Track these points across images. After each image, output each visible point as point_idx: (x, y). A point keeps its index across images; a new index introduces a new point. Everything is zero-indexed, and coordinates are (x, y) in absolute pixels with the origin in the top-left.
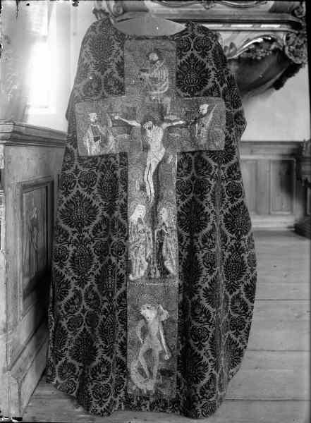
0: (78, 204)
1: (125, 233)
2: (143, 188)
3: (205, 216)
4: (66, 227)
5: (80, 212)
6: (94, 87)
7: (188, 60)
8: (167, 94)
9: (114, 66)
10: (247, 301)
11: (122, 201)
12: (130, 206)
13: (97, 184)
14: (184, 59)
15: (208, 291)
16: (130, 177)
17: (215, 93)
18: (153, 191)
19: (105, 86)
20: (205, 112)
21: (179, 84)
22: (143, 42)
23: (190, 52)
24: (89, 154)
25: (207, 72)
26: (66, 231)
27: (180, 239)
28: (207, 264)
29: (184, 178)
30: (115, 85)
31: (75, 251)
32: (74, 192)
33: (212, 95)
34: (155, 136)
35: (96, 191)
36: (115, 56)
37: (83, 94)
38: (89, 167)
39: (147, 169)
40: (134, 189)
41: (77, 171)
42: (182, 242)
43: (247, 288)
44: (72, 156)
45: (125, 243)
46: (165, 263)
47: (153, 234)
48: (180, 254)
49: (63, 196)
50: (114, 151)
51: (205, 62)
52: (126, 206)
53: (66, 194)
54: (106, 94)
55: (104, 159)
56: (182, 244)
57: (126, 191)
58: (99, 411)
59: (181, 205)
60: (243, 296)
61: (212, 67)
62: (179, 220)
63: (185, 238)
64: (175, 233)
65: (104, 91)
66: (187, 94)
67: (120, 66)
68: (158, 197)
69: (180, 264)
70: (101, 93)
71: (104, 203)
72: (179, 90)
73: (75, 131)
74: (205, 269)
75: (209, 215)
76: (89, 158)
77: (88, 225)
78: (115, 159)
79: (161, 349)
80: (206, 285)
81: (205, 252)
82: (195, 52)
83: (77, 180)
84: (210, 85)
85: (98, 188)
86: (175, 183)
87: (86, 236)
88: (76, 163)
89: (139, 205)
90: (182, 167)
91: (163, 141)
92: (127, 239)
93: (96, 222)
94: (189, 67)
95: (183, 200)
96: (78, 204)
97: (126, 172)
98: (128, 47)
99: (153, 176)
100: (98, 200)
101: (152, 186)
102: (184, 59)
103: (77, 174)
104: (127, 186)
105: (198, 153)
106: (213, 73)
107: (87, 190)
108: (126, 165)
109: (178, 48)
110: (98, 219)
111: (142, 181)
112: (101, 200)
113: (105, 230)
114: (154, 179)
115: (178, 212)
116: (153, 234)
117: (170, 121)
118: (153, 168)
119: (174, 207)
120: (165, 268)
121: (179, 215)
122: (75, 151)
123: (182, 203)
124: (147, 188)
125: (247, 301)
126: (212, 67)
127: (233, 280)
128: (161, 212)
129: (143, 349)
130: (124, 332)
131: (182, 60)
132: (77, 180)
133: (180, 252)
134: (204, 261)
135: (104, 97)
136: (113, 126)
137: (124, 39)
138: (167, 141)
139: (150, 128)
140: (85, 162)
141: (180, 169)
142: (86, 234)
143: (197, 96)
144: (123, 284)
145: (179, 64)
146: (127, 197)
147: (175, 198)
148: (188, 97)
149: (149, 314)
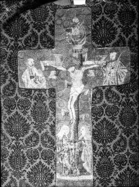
0: (17, 120)
1: (54, 145)
2: (67, 114)
4: (8, 135)
5: (17, 126)
6: (32, 40)
7: (100, 22)
8: (85, 46)
9: (48, 28)
11: (52, 123)
12: (57, 126)
13: (31, 109)
14: (98, 20)
15: (118, 181)
16: (57, 106)
18: (75, 116)
19: (41, 40)
20: (114, 58)
21: (94, 38)
22: (68, 10)
23: (101, 15)
24: (26, 87)
26: (6, 39)
27: (94, 148)
28: (117, 162)
29: (97, 105)
30: (49, 141)
31: (13, 153)
32: (14, 112)
33: (118, 46)
34: (77, 75)
35: (29, 114)
36: (50, 121)
37: (24, 44)
38: (25, 96)
39: (70, 100)
40: (61, 114)
41: (17, 98)
42: (96, 150)
44: (15, 87)
45: (54, 152)
48: (94, 159)
49: (7, 113)
50: (45, 87)
51: (113, 22)
52: (55, 126)
53: (9, 112)
54: (42, 47)
55: (37, 92)
56: (96, 152)
57: (55, 115)
59: (95, 124)
61: (118, 25)
62: (93, 134)
63: (98, 147)
64: (90, 144)
65: (40, 44)
66: (100, 45)
67: (52, 28)
68: (78, 120)
69: (94, 165)
70: (38, 45)
71: (35, 122)
72: (94, 43)
73: (17, 70)
74: (116, 166)
75: (118, 130)
76: (26, 89)
77: (22, 36)
78: (45, 93)
80: (117, 176)
81: (116, 155)
82: (105, 15)
83: (17, 104)
85: (31, 111)
86: (90, 109)
87: (20, 44)
88: (17, 92)
89: (64, 126)
90: (96, 98)
91: (83, 80)
92: (55, 149)
93: (27, 35)
94: (101, 27)
95: (96, 120)
96: (17, 120)
97: (55, 103)
98: (58, 14)
99: (75, 103)
100: (30, 20)
102: (98, 20)
103: (17, 100)
104: (55, 112)
105: (108, 87)
106: (119, 30)
107: (23, 112)
108: (54, 97)
109: (93, 13)
110: (30, 133)
111: (67, 108)
112: (33, 120)
113: (33, 41)
115: (93, 129)
118: (75, 99)
119: (90, 125)
120: (83, 168)
121: (94, 131)
122: (17, 83)
123: (95, 123)
124: (70, 113)
126: (118, 25)
128: (81, 130)
131: (96, 21)
132: (17, 104)
133: (94, 157)
134: (115, 161)
135: (39, 48)
136: (45, 70)
137: (56, 9)
138: (85, 80)
139: (73, 72)
140: (23, 92)
141: (94, 99)
142: (19, 43)
143: (107, 46)
145: (94, 24)
146: (55, 120)
147: (90, 119)
148: (100, 47)
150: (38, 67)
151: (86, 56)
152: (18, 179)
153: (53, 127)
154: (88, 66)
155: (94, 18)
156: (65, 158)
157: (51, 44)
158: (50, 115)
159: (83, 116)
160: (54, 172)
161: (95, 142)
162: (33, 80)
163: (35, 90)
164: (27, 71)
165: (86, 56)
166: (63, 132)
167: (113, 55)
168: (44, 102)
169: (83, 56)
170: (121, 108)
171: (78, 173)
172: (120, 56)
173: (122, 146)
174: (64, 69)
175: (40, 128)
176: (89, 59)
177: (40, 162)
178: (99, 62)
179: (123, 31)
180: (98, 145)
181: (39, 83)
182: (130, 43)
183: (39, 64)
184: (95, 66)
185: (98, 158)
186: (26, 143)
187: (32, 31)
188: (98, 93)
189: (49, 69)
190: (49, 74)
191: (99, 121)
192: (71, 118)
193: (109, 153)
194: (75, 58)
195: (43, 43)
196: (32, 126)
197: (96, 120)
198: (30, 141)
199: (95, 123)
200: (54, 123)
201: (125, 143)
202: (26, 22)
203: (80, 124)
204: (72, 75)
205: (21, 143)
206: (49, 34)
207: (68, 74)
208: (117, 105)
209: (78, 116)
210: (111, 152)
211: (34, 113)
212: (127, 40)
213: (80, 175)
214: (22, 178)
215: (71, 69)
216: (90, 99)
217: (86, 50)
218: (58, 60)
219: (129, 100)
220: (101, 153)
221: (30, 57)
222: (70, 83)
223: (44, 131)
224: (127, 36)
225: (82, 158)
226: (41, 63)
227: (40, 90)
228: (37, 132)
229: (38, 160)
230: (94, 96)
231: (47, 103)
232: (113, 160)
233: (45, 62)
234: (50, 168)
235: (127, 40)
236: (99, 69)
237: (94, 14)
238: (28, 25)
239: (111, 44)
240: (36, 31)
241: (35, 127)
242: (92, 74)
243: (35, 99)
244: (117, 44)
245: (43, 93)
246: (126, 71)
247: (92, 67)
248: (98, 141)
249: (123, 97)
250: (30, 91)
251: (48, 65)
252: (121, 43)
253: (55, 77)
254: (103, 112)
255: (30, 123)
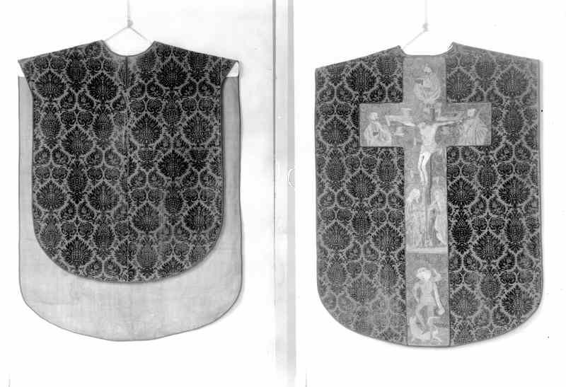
2: (417, 176)
3: (471, 83)
8: (439, 100)
10: (529, 148)
17: (478, 99)
20: (472, 115)
25: (474, 192)
27: (449, 210)
29: (453, 164)
30: (397, 201)
32: (358, 171)
42: (451, 213)
43: (527, 137)
46: (437, 235)
47: (427, 212)
48: (449, 222)
58: (378, 335)
59: (450, 185)
60: (525, 145)
62: (448, 196)
68: (431, 183)
79: (435, 305)
84: (474, 92)
87: (494, 267)
95: (452, 180)
101: (426, 173)
103: (361, 158)
114: (427, 169)
116: (427, 212)
117: (439, 122)
123: (450, 183)
124: (421, 175)
125: (529, 148)
127: (516, 241)
129: (419, 307)
130: (403, 281)
141: (449, 157)
142: (465, 211)
143: (463, 101)
144: (402, 244)
148: (455, 102)
149: (424, 274)
150: (383, 122)
151: (438, 111)
152: (362, 244)
153: (401, 188)
154: (442, 122)
155: (448, 71)
156: (415, 228)
157: (399, 97)
158: (399, 173)
159: (436, 179)
160: (402, 235)
161: (450, 204)
162: (376, 137)
163: (382, 148)
164: (370, 127)
165: (438, 111)
166: (413, 195)
167: (471, 112)
168: (392, 160)
169: (436, 111)
170: (480, 167)
171: (431, 244)
172: (479, 113)
173: (482, 209)
174: (413, 125)
175: (387, 188)
176: (443, 115)
177: (388, 225)
178: (456, 118)
179: (481, 83)
180: (453, 207)
181: (383, 140)
182: (488, 97)
183: (384, 119)
184: (450, 123)
185: (454, 222)
186: (372, 204)
187: (191, 170)
188: (453, 152)
189: (394, 125)
190: (395, 130)
191: (454, 181)
192: (422, 180)
193: (466, 216)
194: (426, 113)
195: (391, 97)
196: (378, 186)
197: (452, 180)
198: (376, 202)
199: (450, 183)
200: (403, 181)
201: (485, 205)
202: (372, 75)
203: (433, 187)
204: (422, 132)
205: (366, 205)
206: (398, 87)
207: (417, 130)
208: (475, 164)
209: (431, 179)
210: (468, 215)
211: (380, 172)
212: (485, 94)
213: (434, 247)
214: (367, 242)
215: (420, 126)
216: (445, 161)
217: (440, 104)
218: (406, 115)
219: (489, 158)
220: (457, 216)
221: (372, 111)
222: (419, 141)
223: (391, 191)
224: (485, 90)
225: (436, 227)
226: (386, 117)
227: (387, 148)
228: (384, 192)
229: (385, 223)
230: (449, 155)
231: (395, 160)
232: (471, 225)
233: (391, 116)
234: (399, 231)
235: (485, 94)
236: (454, 125)
237: (449, 67)
238: (374, 78)
239: (467, 99)
240: (384, 85)
241: (381, 187)
242: (446, 131)
243: (382, 157)
244: (473, 99)
245: (390, 150)
246: (487, 130)
247: (444, 124)
248: (454, 203)
249: (482, 155)
250: (375, 149)
251: (394, 120)
252: (478, 98)
253: (402, 135)
254: (459, 172)
255: (376, 182)
